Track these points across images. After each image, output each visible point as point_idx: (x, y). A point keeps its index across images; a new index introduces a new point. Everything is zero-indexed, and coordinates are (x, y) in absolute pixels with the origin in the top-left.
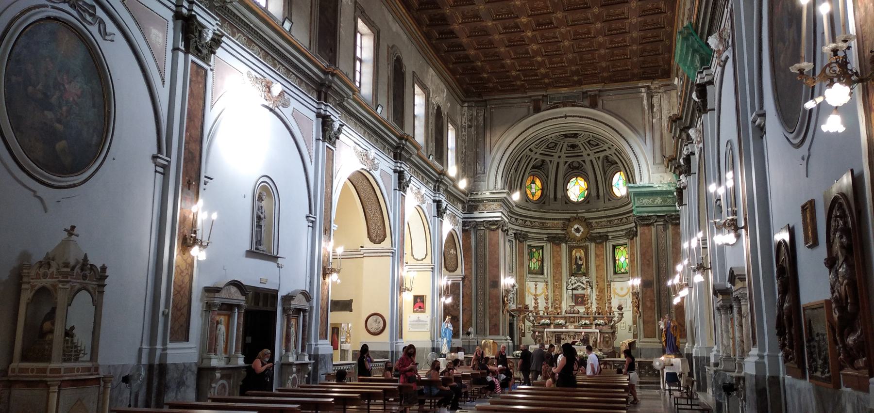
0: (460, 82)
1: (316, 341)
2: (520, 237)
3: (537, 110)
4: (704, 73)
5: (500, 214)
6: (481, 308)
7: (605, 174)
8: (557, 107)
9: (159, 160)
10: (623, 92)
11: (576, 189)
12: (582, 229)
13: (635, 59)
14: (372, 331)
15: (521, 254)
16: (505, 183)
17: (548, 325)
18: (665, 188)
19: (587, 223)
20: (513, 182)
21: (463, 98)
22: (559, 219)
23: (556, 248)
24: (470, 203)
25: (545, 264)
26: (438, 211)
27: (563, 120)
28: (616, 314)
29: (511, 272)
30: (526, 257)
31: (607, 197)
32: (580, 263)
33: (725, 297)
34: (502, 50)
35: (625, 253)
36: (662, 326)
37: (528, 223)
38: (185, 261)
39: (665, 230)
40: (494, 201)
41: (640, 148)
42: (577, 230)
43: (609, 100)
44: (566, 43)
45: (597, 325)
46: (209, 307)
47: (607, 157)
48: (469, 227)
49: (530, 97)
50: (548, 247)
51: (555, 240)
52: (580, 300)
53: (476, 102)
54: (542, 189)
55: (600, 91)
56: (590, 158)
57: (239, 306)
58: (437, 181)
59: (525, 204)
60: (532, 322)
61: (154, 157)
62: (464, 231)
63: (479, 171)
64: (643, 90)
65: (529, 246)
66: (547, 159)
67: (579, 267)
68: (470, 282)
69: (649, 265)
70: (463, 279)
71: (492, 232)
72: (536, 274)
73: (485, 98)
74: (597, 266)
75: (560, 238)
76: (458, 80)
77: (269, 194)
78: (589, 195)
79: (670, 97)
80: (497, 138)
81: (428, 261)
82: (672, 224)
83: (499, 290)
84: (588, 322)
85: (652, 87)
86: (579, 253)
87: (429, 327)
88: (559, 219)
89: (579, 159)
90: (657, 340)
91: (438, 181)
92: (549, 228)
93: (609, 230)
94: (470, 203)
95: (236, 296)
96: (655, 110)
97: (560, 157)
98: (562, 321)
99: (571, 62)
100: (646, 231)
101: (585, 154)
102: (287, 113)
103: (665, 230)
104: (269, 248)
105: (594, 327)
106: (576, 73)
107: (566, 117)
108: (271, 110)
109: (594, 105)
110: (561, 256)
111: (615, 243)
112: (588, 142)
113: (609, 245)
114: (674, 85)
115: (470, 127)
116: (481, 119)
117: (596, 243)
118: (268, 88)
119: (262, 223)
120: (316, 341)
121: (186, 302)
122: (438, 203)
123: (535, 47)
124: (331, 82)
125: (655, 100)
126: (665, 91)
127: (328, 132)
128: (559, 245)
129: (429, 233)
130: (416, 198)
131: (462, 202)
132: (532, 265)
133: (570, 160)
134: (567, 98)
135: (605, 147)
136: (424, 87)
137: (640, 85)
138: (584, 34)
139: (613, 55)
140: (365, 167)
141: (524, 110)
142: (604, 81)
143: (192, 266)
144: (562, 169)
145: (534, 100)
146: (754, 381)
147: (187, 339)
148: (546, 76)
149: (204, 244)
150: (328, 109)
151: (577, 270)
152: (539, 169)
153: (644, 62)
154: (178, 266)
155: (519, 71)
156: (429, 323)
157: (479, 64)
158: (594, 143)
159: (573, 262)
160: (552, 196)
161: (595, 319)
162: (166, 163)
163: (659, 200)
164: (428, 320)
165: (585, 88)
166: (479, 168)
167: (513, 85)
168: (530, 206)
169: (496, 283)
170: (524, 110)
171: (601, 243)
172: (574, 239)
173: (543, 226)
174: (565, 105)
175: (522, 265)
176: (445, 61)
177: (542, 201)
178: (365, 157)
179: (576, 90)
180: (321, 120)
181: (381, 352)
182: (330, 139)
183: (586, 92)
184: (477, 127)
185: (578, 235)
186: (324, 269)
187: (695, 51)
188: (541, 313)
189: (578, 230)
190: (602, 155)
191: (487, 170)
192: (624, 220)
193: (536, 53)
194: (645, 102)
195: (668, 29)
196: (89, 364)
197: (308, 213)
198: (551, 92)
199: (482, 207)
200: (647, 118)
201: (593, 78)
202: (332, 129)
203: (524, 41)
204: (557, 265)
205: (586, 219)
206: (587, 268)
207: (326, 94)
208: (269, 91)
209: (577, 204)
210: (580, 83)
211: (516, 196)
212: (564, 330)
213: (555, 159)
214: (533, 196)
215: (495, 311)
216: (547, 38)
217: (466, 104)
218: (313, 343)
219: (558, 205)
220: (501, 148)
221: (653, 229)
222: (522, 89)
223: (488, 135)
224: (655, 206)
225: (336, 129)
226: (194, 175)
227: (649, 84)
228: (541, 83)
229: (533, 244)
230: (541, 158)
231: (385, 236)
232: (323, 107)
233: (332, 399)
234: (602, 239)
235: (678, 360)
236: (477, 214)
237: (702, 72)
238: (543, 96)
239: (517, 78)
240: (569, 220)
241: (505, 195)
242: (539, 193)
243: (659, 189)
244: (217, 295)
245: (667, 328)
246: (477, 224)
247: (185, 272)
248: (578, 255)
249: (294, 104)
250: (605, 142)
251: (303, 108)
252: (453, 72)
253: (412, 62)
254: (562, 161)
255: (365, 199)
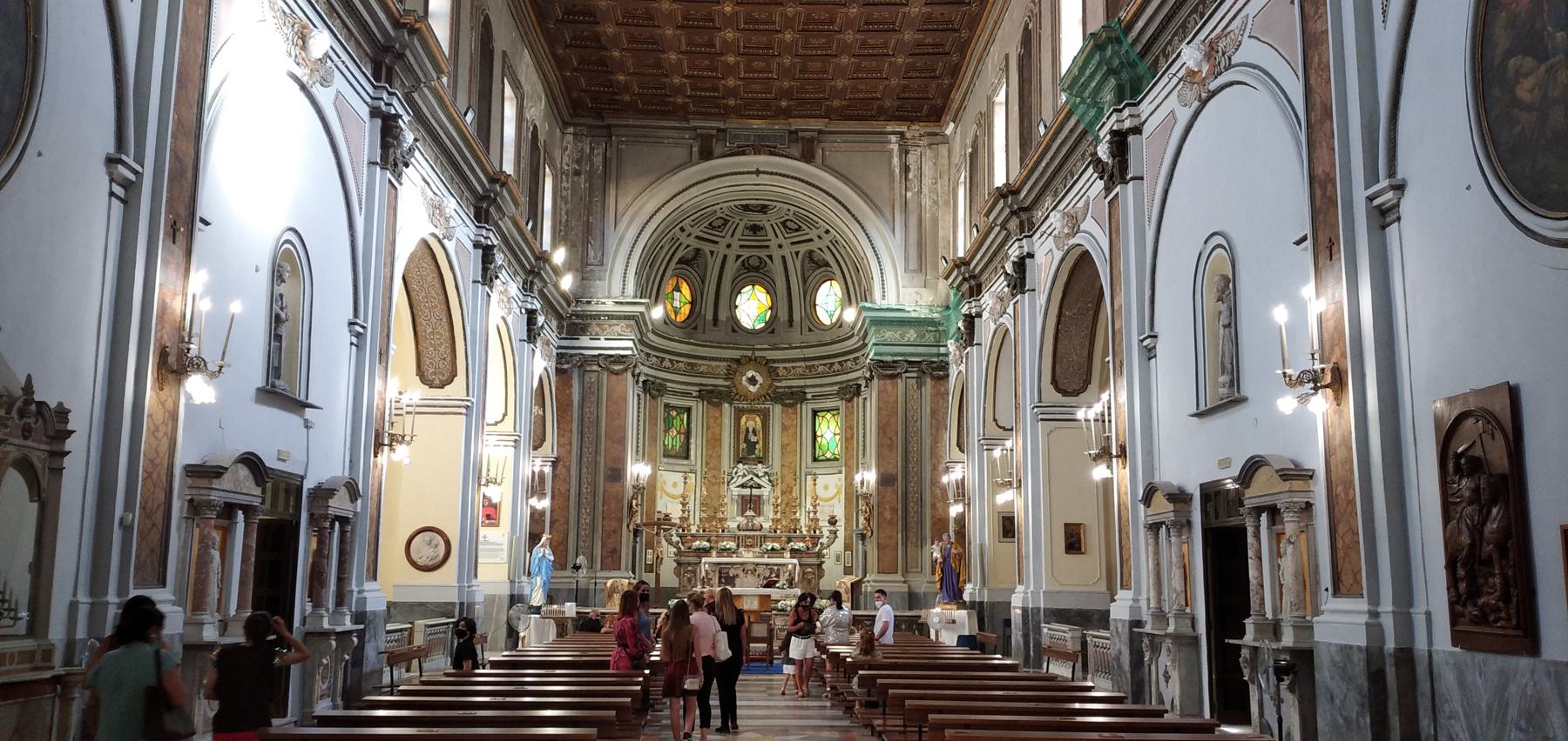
0: (568, 85)
1: (360, 584)
2: (652, 389)
3: (707, 155)
4: (1126, 112)
5: (630, 344)
6: (586, 519)
7: (805, 282)
8: (743, 153)
9: (121, 168)
10: (851, 138)
11: (752, 307)
12: (759, 379)
13: (894, 82)
14: (420, 562)
15: (653, 419)
16: (638, 284)
17: (706, 552)
18: (923, 313)
19: (768, 367)
20: (651, 288)
21: (567, 118)
22: (720, 359)
23: (714, 412)
24: (574, 322)
25: (692, 441)
26: (529, 331)
27: (753, 179)
28: (826, 533)
29: (642, 455)
30: (661, 425)
31: (806, 323)
32: (753, 439)
33: (1179, 506)
34: (669, 32)
35: (833, 425)
36: (937, 555)
37: (667, 364)
38: (163, 404)
39: (920, 387)
40: (619, 318)
41: (884, 239)
42: (752, 381)
43: (837, 150)
44: (788, 37)
45: (793, 550)
46: (195, 508)
47: (811, 252)
48: (568, 365)
49: (695, 129)
50: (698, 409)
51: (712, 397)
52: (751, 503)
53: (590, 127)
54: (693, 303)
55: (820, 132)
56: (726, 251)
57: (248, 510)
58: (531, 272)
59: (664, 328)
60: (676, 545)
61: (111, 161)
62: (559, 371)
63: (592, 260)
64: (893, 138)
65: (667, 406)
66: (707, 248)
67: (751, 446)
68: (568, 469)
69: (891, 447)
70: (555, 464)
71: (614, 377)
72: (674, 457)
73: (608, 121)
74: (784, 447)
75: (720, 393)
76: (566, 81)
77: (295, 271)
78: (774, 318)
79: (936, 157)
80: (629, 200)
81: (507, 426)
82: (933, 377)
83: (623, 486)
84: (777, 545)
85: (908, 135)
86: (752, 422)
87: (505, 555)
88: (720, 359)
89: (763, 254)
90: (899, 577)
91: (534, 272)
92: (701, 375)
93: (809, 382)
94: (575, 321)
95: (241, 485)
96: (911, 175)
97: (729, 246)
98: (732, 545)
99: (785, 72)
100: (889, 387)
101: (773, 243)
102: (325, 96)
103: (920, 387)
104: (291, 383)
105: (788, 554)
106: (787, 94)
107: (758, 172)
108: (303, 87)
109: (808, 157)
110: (720, 426)
111: (816, 406)
112: (784, 223)
113: (807, 409)
114: (944, 136)
115: (577, 173)
116: (598, 160)
117: (784, 405)
118: (303, 39)
119: (284, 330)
120: (360, 584)
121: (161, 496)
122: (531, 314)
123: (730, 35)
124: (404, 46)
125: (912, 159)
126: (930, 145)
127: (390, 156)
128: (718, 405)
129: (515, 369)
130: (503, 305)
131: (560, 317)
132: (668, 441)
133: (746, 253)
134: (761, 138)
135: (813, 234)
136: (517, 86)
137: (889, 129)
138: (822, 23)
139: (858, 69)
140: (437, 232)
141: (680, 153)
142: (829, 114)
143: (174, 416)
144: (732, 267)
145: (701, 136)
146: (1363, 656)
147: (164, 585)
148: (733, 92)
149: (212, 367)
150: (395, 102)
151: (749, 452)
152: (691, 264)
153: (905, 88)
154: (150, 416)
155: (687, 77)
156: (505, 547)
157: (616, 54)
158: (794, 225)
159: (742, 437)
160: (709, 319)
161: (789, 540)
162: (132, 177)
163: (911, 335)
164: (505, 541)
165: (797, 124)
166: (591, 253)
167: (667, 104)
168: (671, 331)
169: (617, 474)
170: (680, 153)
171: (792, 406)
172: (745, 396)
173: (692, 370)
174: (757, 152)
175: (654, 439)
176: (551, 40)
177: (692, 325)
178: (436, 209)
179: (779, 126)
180: (379, 122)
181: (438, 605)
182: (396, 165)
183: (796, 132)
184: (590, 175)
185: (752, 389)
186: (378, 435)
187: (1112, 72)
188: (694, 530)
189: (752, 381)
190: (803, 248)
191: (609, 260)
192: (837, 367)
193: (728, 47)
194: (896, 160)
195: (964, 34)
196: (29, 644)
197: (351, 316)
198: (733, 124)
199: (595, 329)
200: (897, 191)
201: (806, 105)
202: (400, 145)
203: (712, 20)
204: (714, 442)
205: (768, 361)
206: (766, 448)
207: (390, 71)
208: (304, 47)
209: (753, 333)
210: (787, 114)
211: (657, 313)
212: (734, 559)
213: (721, 250)
214: (676, 314)
215: (614, 524)
216: (756, 22)
217: (571, 130)
218: (354, 587)
219: (719, 334)
220: (637, 216)
221: (900, 383)
222: (682, 113)
223: (612, 192)
224: (905, 343)
225: (406, 146)
226: (183, 212)
227: (904, 129)
228: (718, 106)
229: (674, 401)
230: (695, 244)
231: (454, 374)
232: (385, 95)
233: (613, 713)
234: (793, 398)
235: (964, 613)
236: (585, 341)
237: (1120, 111)
238: (719, 130)
239: (680, 90)
240: (738, 361)
241: (642, 309)
242: (686, 310)
243: (913, 315)
244: (216, 484)
245: (945, 558)
246: (586, 360)
247: (162, 428)
248: (751, 425)
249: (339, 82)
250: (813, 224)
251: (349, 93)
252: (561, 64)
253: (505, 36)
254: (732, 254)
255: (420, 297)
